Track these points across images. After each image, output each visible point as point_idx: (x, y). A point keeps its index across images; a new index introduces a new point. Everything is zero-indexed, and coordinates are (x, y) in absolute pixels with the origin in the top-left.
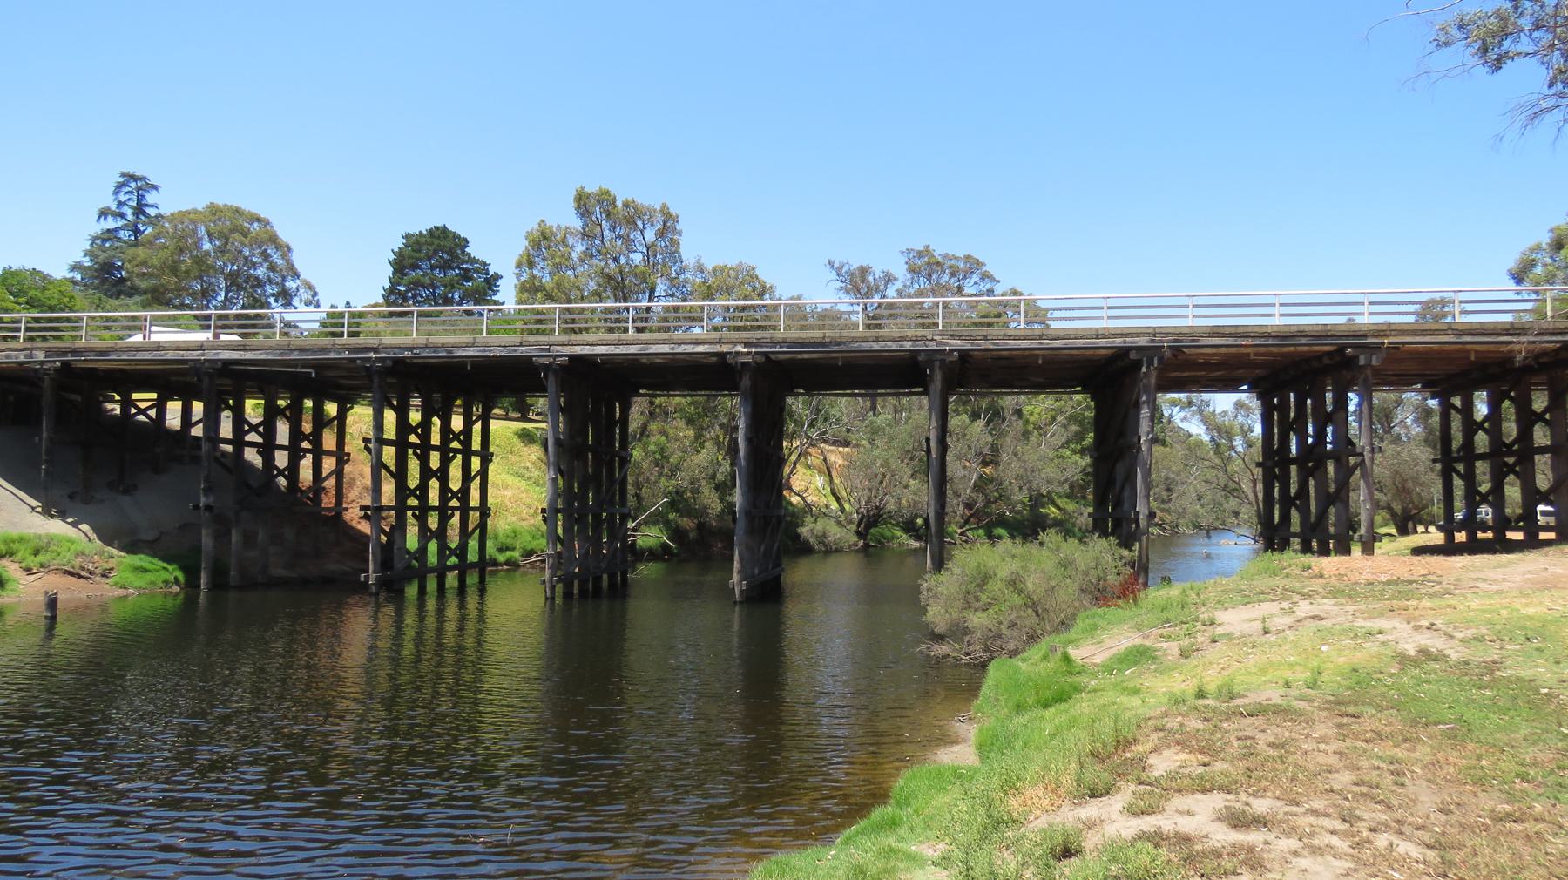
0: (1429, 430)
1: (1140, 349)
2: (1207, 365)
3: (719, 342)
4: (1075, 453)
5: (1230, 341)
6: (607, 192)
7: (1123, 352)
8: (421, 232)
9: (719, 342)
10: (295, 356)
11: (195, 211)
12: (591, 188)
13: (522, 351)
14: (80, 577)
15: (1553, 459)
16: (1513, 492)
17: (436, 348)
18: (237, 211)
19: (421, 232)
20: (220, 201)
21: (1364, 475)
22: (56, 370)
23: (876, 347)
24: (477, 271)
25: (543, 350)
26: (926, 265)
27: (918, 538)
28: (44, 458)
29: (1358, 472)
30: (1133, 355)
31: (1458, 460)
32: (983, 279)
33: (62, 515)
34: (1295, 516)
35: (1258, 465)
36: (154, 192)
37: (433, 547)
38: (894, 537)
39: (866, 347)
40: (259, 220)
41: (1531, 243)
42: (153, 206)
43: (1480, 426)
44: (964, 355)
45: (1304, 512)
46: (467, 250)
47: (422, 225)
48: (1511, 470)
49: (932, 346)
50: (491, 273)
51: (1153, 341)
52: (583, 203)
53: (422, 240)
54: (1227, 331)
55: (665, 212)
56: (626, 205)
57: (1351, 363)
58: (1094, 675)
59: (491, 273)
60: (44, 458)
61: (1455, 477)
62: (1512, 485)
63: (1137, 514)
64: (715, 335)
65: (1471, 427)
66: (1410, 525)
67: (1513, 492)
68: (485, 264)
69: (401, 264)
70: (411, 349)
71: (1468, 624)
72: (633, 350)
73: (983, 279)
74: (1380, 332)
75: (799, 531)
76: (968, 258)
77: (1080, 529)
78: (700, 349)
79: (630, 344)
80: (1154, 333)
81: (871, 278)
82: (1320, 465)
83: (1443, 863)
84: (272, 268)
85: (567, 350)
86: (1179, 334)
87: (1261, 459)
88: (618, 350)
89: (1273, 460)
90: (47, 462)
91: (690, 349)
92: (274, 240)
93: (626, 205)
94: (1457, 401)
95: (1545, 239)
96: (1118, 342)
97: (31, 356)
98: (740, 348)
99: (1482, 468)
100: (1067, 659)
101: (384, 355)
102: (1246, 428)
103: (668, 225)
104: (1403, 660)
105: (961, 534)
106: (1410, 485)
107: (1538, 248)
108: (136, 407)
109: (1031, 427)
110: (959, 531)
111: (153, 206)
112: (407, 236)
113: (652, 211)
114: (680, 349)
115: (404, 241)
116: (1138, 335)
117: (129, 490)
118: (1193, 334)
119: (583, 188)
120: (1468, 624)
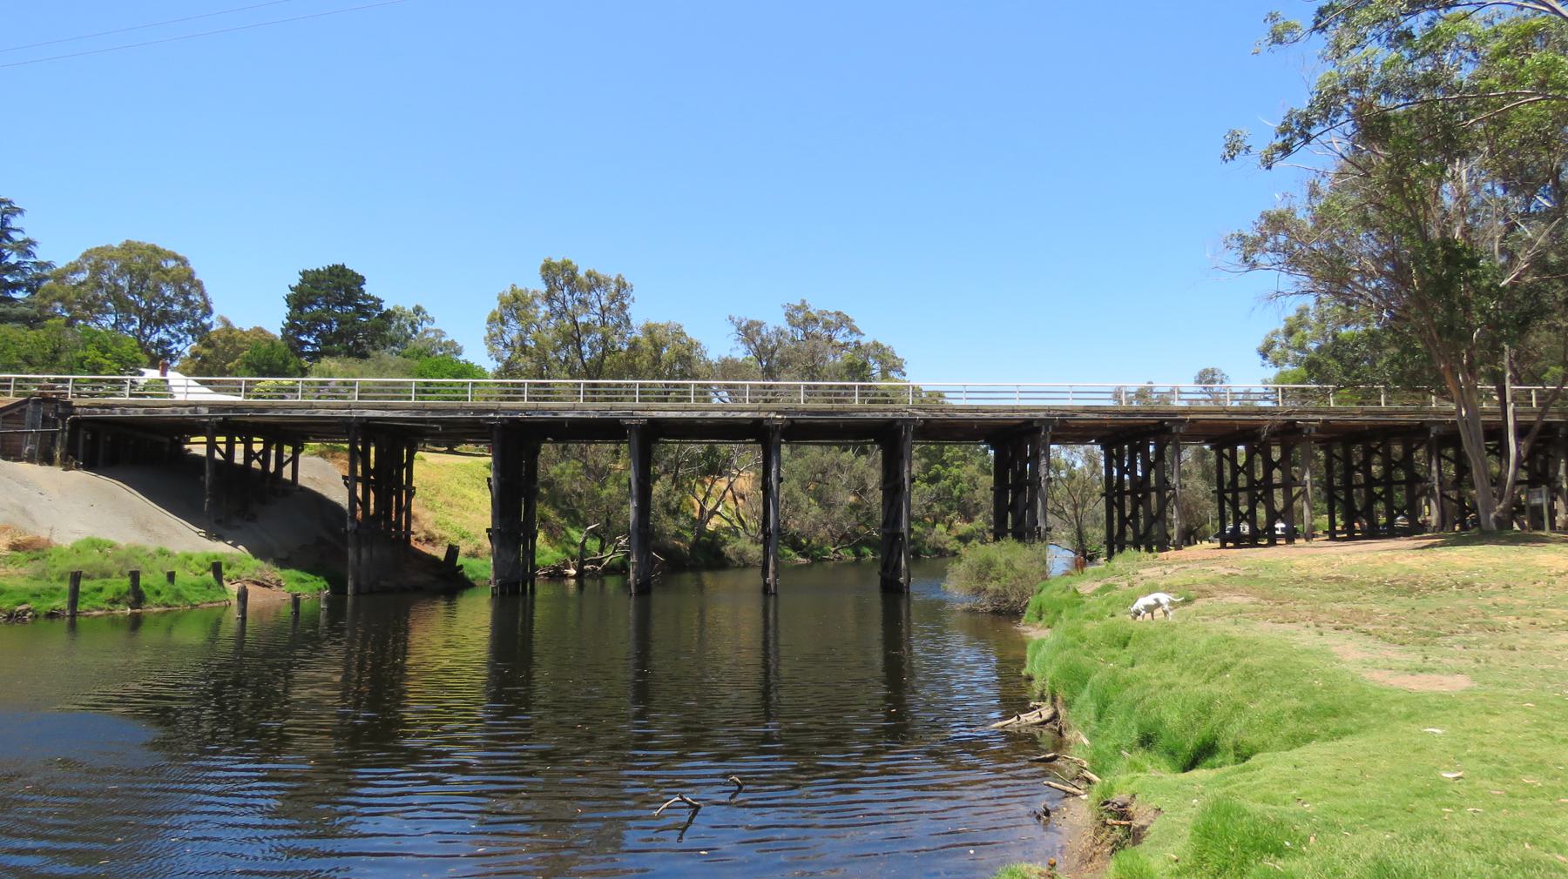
0: (1206, 468)
1: (1041, 420)
2: (1077, 428)
3: (759, 410)
4: (923, 482)
5: (1096, 416)
6: (570, 263)
7: (1029, 422)
8: (318, 270)
9: (759, 410)
10: (428, 415)
11: (109, 248)
12: (557, 260)
13: (613, 414)
14: (264, 586)
15: (1284, 491)
16: (1261, 513)
17: (544, 411)
18: (155, 250)
19: (318, 270)
20: (135, 239)
21: (1176, 503)
22: (218, 423)
23: (868, 416)
24: (370, 307)
25: (628, 414)
26: (802, 317)
27: (804, 555)
28: (208, 493)
29: (1172, 501)
30: (1036, 424)
31: (1227, 491)
32: (851, 333)
33: (220, 538)
34: (1129, 529)
35: (991, 489)
36: (18, 215)
37: (1244, 509)
38: (785, 555)
39: (861, 415)
40: (176, 258)
41: (1273, 328)
42: (18, 230)
43: (1241, 469)
44: (927, 421)
45: (1135, 527)
46: (363, 287)
47: (321, 263)
48: (1260, 498)
49: (906, 415)
50: (385, 309)
51: (1048, 415)
52: (550, 272)
53: (321, 277)
54: (1093, 409)
55: (622, 285)
56: (589, 275)
57: (1167, 430)
58: (1089, 597)
59: (385, 309)
60: (208, 493)
61: (1226, 502)
62: (1260, 507)
63: (1039, 529)
64: (755, 406)
65: (1236, 470)
66: (1192, 538)
67: (1261, 513)
68: (380, 301)
69: (298, 300)
70: (524, 411)
71: (1246, 565)
72: (695, 415)
73: (851, 333)
74: (1184, 412)
75: (723, 549)
76: (838, 314)
77: (929, 547)
78: (745, 415)
79: (668, 411)
80: (1048, 409)
81: (764, 333)
82: (1147, 496)
83: (1237, 655)
84: (187, 303)
85: (647, 414)
86: (1064, 410)
87: (653, 445)
88: (684, 415)
89: (1113, 493)
90: (210, 495)
91: (738, 415)
92: (190, 277)
93: (589, 275)
94: (1226, 451)
95: (1281, 327)
96: (1027, 415)
97: (195, 411)
98: (772, 415)
99: (1243, 497)
100: (1076, 591)
101: (502, 416)
102: (1070, 463)
103: (622, 289)
104: (1224, 577)
105: (835, 552)
106: (1193, 508)
107: (1275, 333)
108: (1404, 515)
109: (10, 344)
110: (833, 549)
111: (18, 230)
112: (304, 274)
113: (607, 282)
114: (729, 415)
115: (301, 277)
116: (1039, 411)
117: (253, 518)
118: (1073, 411)
119: (550, 259)
120: (1246, 565)
